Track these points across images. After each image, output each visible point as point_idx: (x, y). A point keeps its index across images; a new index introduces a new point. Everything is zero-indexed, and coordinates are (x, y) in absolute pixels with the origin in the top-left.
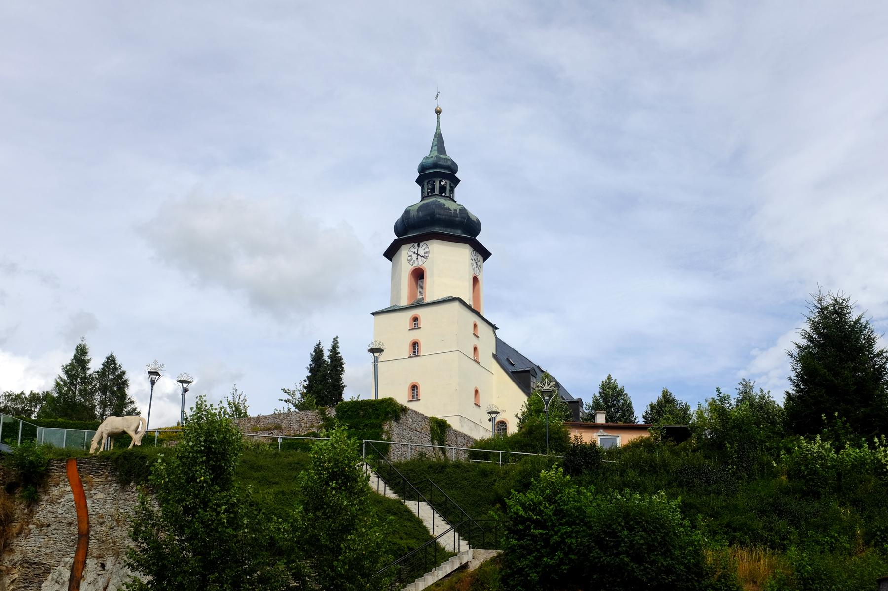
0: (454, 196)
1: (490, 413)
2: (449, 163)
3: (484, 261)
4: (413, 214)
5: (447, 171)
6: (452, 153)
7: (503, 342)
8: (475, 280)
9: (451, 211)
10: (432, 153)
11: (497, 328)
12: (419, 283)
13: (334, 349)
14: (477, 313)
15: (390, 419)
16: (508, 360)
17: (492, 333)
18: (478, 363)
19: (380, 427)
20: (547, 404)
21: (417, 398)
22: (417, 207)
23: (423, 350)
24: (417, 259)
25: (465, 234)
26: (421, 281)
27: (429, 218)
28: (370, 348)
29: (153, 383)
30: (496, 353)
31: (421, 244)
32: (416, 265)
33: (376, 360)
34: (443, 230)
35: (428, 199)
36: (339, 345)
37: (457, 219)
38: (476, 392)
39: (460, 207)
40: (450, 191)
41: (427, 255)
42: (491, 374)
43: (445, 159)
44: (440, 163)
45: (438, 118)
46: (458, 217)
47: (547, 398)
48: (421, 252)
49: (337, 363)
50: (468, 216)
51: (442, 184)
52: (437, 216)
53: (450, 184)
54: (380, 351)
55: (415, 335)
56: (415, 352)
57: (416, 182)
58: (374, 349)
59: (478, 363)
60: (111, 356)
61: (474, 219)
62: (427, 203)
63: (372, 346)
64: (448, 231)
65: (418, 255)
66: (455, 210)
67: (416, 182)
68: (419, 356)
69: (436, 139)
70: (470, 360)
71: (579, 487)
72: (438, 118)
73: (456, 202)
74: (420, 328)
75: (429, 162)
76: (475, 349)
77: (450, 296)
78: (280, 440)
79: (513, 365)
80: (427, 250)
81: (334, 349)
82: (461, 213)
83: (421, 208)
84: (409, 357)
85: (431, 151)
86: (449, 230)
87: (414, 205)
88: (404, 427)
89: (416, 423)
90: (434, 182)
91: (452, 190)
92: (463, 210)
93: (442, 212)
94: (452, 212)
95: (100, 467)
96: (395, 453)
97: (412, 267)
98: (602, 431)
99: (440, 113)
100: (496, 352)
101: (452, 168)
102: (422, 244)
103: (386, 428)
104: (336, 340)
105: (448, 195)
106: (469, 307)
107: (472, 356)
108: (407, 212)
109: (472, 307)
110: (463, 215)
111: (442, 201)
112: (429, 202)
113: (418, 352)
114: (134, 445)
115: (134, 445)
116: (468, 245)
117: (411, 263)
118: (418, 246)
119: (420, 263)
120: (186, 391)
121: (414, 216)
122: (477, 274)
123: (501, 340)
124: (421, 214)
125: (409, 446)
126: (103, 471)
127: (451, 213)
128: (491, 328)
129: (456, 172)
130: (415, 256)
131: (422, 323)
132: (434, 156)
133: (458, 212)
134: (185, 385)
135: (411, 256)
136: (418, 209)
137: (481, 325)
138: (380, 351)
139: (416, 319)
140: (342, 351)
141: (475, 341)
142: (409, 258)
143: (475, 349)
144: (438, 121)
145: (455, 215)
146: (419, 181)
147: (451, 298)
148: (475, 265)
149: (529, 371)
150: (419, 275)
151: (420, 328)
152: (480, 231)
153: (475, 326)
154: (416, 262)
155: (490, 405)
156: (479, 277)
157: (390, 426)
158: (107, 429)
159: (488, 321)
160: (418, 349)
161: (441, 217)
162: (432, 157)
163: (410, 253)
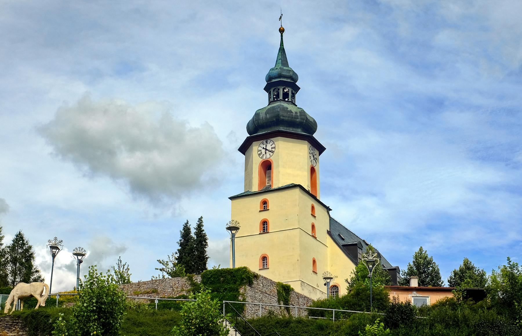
0: (295, 101)
1: (325, 278)
2: (291, 73)
4: (262, 116)
5: (289, 80)
6: (293, 64)
7: (335, 221)
9: (293, 113)
10: (277, 65)
12: (267, 173)
13: (200, 227)
14: (314, 198)
15: (245, 284)
16: (339, 235)
17: (326, 213)
18: (316, 238)
19: (237, 290)
20: (371, 271)
22: (265, 111)
23: (271, 228)
24: (266, 153)
28: (229, 226)
29: (54, 256)
30: (330, 230)
31: (269, 141)
33: (233, 236)
36: (203, 224)
37: (298, 120)
38: (314, 262)
41: (273, 150)
42: (326, 247)
44: (283, 73)
45: (282, 36)
46: (298, 118)
48: (269, 147)
49: (201, 238)
51: (285, 91)
52: (282, 117)
53: (292, 91)
54: (237, 229)
55: (264, 215)
56: (264, 230)
59: (316, 238)
60: (20, 234)
63: (229, 224)
65: (266, 149)
66: (296, 113)
68: (268, 232)
72: (282, 36)
73: (296, 106)
74: (268, 210)
75: (274, 73)
76: (313, 226)
78: (156, 302)
79: (343, 239)
80: (273, 146)
81: (200, 227)
82: (301, 115)
83: (268, 111)
84: (260, 234)
87: (262, 109)
88: (256, 291)
90: (279, 89)
92: (303, 113)
93: (285, 114)
94: (294, 114)
95: (12, 324)
97: (262, 160)
98: (415, 292)
100: (330, 229)
101: (294, 78)
103: (241, 291)
104: (200, 220)
105: (290, 100)
106: (307, 192)
108: (257, 115)
110: (303, 117)
111: (285, 105)
112: (275, 106)
113: (267, 229)
114: (40, 306)
115: (40, 306)
117: (261, 156)
118: (267, 142)
119: (268, 156)
120: (80, 262)
122: (314, 165)
125: (261, 306)
126: (15, 328)
128: (326, 210)
129: (297, 81)
130: (263, 151)
131: (270, 206)
132: (278, 68)
133: (298, 114)
134: (80, 258)
135: (261, 150)
137: (317, 207)
138: (237, 229)
140: (206, 229)
141: (312, 220)
142: (259, 152)
143: (313, 226)
144: (282, 39)
146: (267, 89)
148: (312, 158)
149: (356, 245)
150: (267, 166)
153: (313, 208)
154: (265, 156)
155: (83, 249)
156: (316, 168)
157: (245, 290)
158: (18, 293)
160: (267, 227)
161: (285, 118)
162: (277, 69)
163: (260, 149)
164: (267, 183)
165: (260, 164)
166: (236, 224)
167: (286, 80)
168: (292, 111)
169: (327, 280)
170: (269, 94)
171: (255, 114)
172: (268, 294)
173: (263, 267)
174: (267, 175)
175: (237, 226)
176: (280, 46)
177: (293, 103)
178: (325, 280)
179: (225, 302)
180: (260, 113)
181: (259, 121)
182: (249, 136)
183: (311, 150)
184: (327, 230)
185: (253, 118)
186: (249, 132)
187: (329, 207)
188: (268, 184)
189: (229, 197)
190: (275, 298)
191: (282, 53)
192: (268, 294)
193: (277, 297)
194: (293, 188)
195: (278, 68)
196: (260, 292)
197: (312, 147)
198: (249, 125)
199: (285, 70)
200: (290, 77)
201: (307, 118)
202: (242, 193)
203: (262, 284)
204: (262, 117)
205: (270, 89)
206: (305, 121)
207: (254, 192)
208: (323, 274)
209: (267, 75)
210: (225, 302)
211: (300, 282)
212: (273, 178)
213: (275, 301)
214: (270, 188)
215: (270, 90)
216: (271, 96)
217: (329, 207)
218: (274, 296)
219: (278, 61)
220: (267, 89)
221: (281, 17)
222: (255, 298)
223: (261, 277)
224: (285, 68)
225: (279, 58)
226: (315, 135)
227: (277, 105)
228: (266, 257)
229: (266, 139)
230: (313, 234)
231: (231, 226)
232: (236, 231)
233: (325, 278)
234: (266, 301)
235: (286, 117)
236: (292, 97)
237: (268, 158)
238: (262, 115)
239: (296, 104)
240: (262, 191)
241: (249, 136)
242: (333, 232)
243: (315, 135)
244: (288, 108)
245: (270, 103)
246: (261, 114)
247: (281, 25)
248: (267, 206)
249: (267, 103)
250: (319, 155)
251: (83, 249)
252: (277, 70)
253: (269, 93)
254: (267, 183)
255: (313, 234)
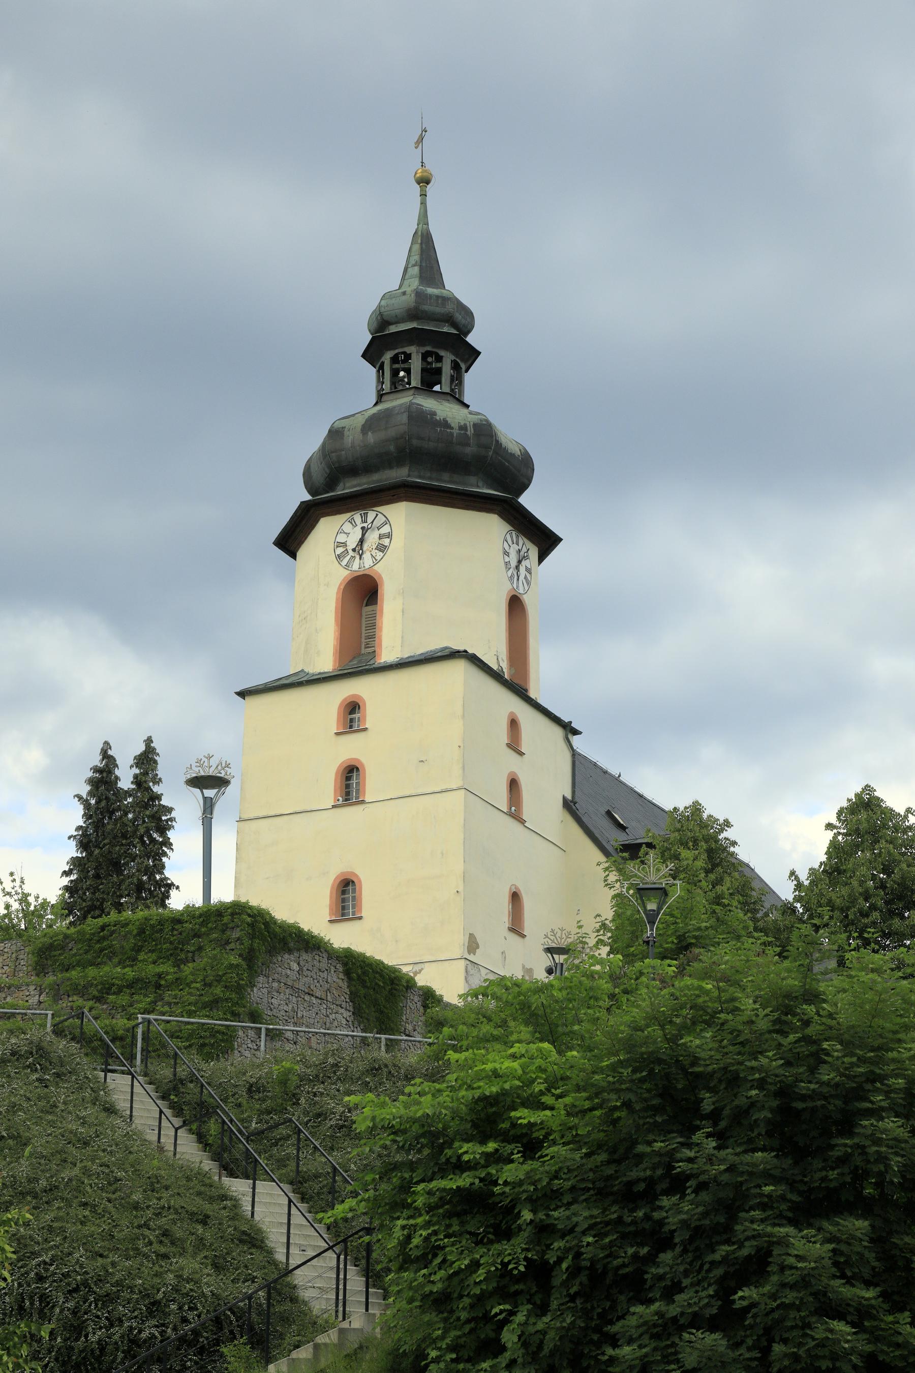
0: (461, 392)
1: (549, 950)
2: (450, 308)
3: (541, 558)
4: (351, 437)
5: (446, 329)
7: (601, 769)
8: (515, 604)
9: (452, 428)
10: (406, 283)
11: (575, 732)
12: (364, 614)
14: (520, 691)
16: (609, 814)
18: (522, 822)
20: (652, 923)
21: (354, 913)
22: (360, 420)
25: (489, 488)
26: (370, 608)
27: (392, 448)
28: (194, 775)
30: (573, 796)
32: (355, 566)
33: (209, 806)
34: (430, 479)
35: (392, 400)
37: (468, 450)
38: (515, 897)
39: (475, 419)
40: (452, 379)
43: (438, 297)
44: (426, 307)
45: (423, 195)
46: (468, 445)
47: (652, 906)
50: (497, 441)
54: (219, 783)
56: (348, 794)
57: (364, 356)
58: (202, 777)
59: (522, 822)
61: (514, 449)
62: (387, 409)
63: (197, 769)
64: (447, 482)
66: (463, 428)
67: (364, 356)
68: (363, 802)
69: (417, 247)
70: (501, 813)
71: (398, 1145)
72: (423, 195)
73: (467, 406)
76: (513, 784)
77: (446, 648)
79: (622, 828)
83: (371, 424)
84: (334, 807)
85: (403, 278)
86: (446, 476)
87: (353, 415)
88: (275, 985)
89: (309, 973)
91: (457, 380)
92: (484, 430)
94: (456, 432)
96: (247, 1053)
97: (346, 573)
99: (428, 182)
100: (573, 792)
102: (374, 514)
105: (447, 389)
106: (496, 676)
107: (502, 802)
108: (335, 434)
109: (506, 677)
111: (428, 403)
112: (395, 407)
113: (358, 791)
116: (496, 516)
117: (344, 562)
121: (353, 442)
122: (521, 591)
123: (595, 764)
124: (371, 438)
127: (452, 434)
128: (558, 732)
129: (469, 332)
131: (371, 716)
132: (408, 290)
133: (471, 431)
136: (363, 426)
138: (219, 783)
139: (353, 708)
141: (511, 763)
142: (340, 550)
143: (513, 784)
144: (423, 203)
145: (464, 440)
147: (446, 652)
151: (365, 729)
152: (530, 482)
153: (514, 724)
155: (553, 931)
156: (527, 599)
159: (555, 716)
160: (358, 784)
162: (404, 293)
164: (363, 646)
165: (342, 587)
166: (206, 764)
167: (436, 327)
168: (449, 420)
169: (556, 956)
170: (378, 371)
171: (330, 431)
172: (317, 997)
173: (343, 915)
174: (364, 620)
175: (222, 775)
176: (418, 225)
177: (455, 398)
178: (549, 955)
179: (143, 1018)
180: (346, 429)
181: (343, 452)
182: (308, 497)
183: (510, 542)
184: (564, 798)
185: (324, 445)
186: (310, 486)
187: (571, 722)
188: (366, 648)
189: (238, 690)
190: (343, 1011)
191: (424, 246)
192: (317, 997)
193: (352, 1009)
194: (449, 659)
195: (408, 290)
196: (287, 991)
197: (514, 533)
198: (310, 466)
199: (431, 296)
200: (449, 319)
201: (498, 444)
202: (281, 679)
203: (298, 964)
204: (350, 441)
205: (381, 355)
206: (491, 453)
207: (320, 673)
208: (546, 936)
209: (373, 313)
210: (143, 1018)
211: (463, 963)
212: (381, 630)
213: (344, 1022)
214: (372, 662)
215: (383, 359)
216: (383, 378)
217: (571, 722)
218: (340, 1006)
219: (409, 270)
220: (371, 354)
221: (421, 139)
222: (271, 1010)
223: (167, 928)
224: (431, 291)
225: (414, 263)
226: (527, 500)
227: (401, 405)
228: (353, 882)
229: (364, 509)
230: (513, 808)
231: (202, 773)
232: (218, 792)
233: (549, 950)
234: (312, 1021)
235: (429, 440)
236: (452, 381)
237: (367, 566)
238: (353, 438)
239: (465, 401)
240: (346, 671)
241: (308, 497)
242: (581, 808)
243: (527, 500)
244: (434, 414)
245: (380, 397)
246: (346, 433)
247: (422, 163)
248: (359, 718)
249: (373, 399)
250: (539, 565)
251: (553, 931)
252: (404, 298)
253: (378, 366)
254: (363, 646)
255: (513, 808)
